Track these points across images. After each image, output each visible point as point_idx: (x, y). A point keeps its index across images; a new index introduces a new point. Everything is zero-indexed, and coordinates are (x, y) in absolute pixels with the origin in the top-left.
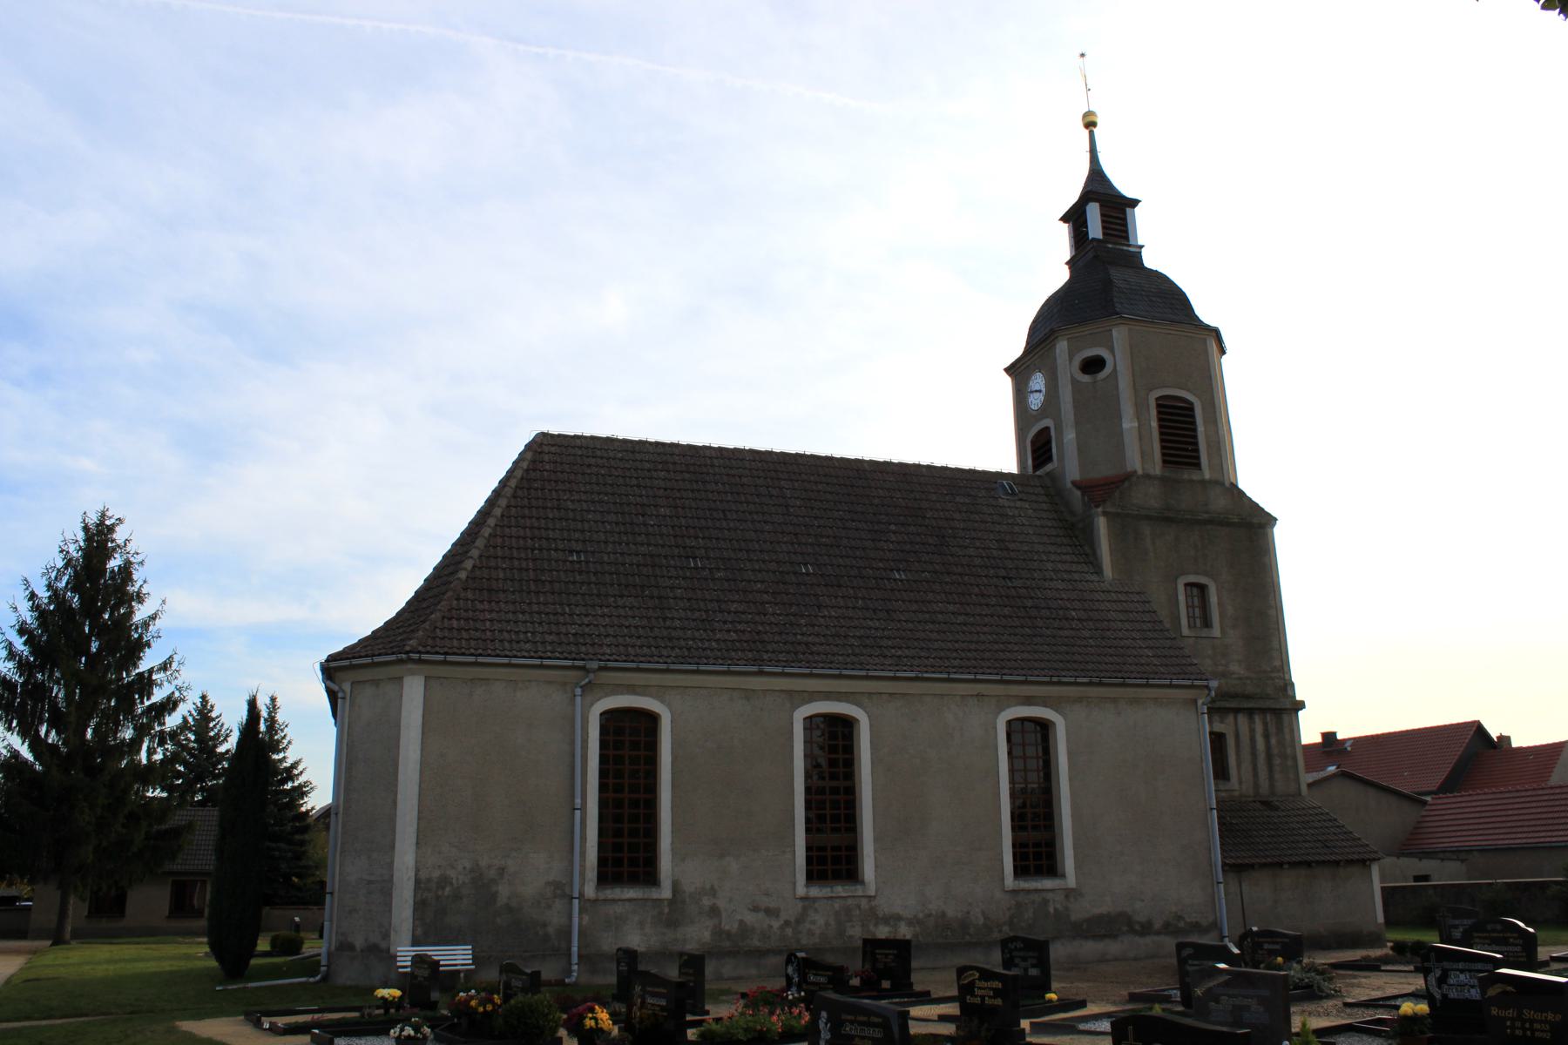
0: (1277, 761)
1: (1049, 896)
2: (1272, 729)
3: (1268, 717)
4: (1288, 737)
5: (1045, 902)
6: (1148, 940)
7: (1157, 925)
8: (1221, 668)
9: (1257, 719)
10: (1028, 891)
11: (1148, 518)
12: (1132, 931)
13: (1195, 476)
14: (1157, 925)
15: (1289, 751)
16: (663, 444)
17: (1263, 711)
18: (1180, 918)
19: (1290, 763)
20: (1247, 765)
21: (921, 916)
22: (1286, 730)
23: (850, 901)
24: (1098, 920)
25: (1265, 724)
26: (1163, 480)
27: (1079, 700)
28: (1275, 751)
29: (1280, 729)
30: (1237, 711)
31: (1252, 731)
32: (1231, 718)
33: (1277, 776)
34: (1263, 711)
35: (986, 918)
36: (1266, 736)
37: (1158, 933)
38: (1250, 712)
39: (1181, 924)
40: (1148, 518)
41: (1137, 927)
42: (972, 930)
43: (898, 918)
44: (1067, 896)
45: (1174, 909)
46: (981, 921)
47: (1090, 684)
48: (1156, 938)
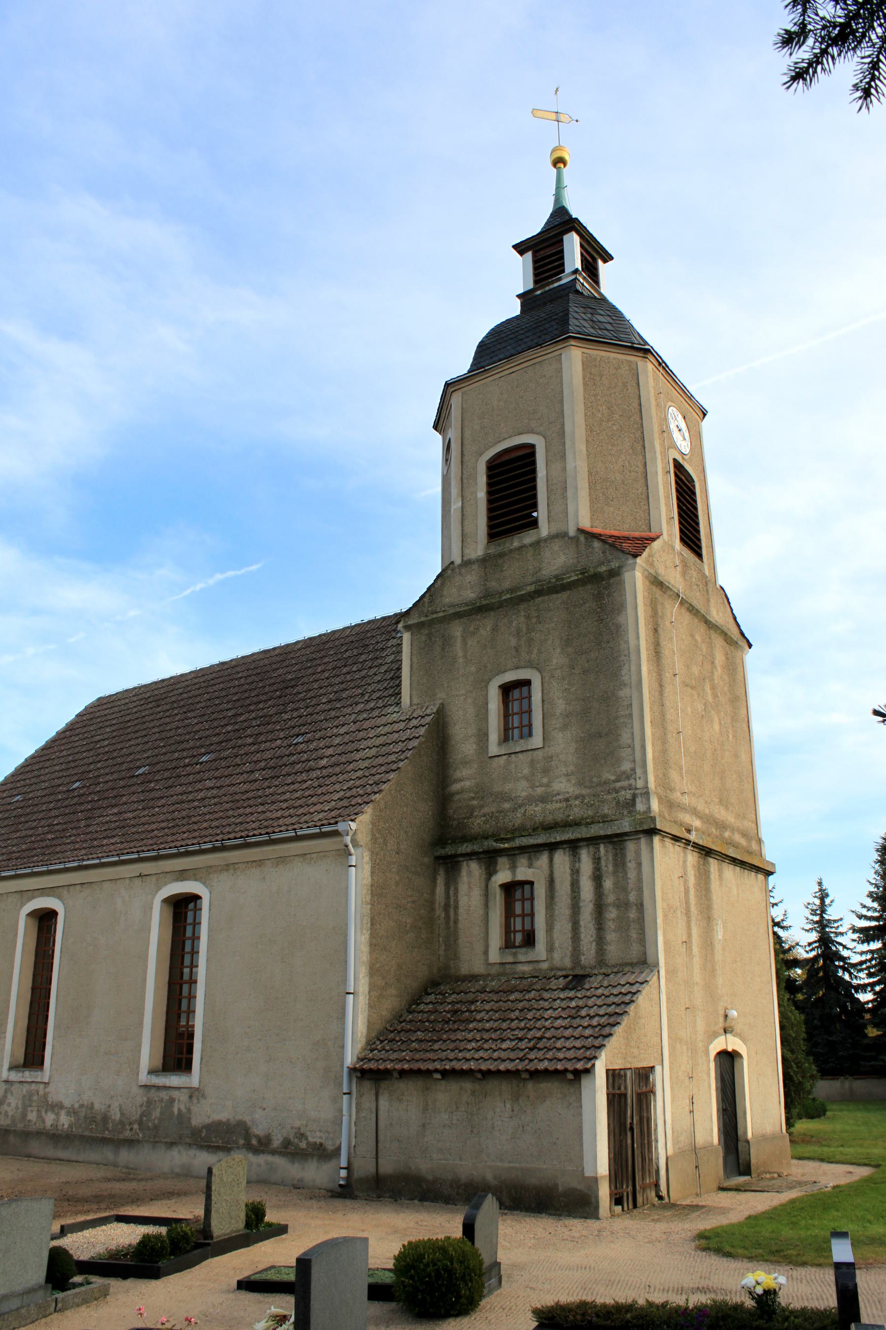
0: (612, 914)
1: (175, 1094)
2: (608, 866)
3: (602, 848)
4: (632, 875)
5: (172, 1100)
6: (262, 1159)
7: (276, 1143)
8: (540, 790)
9: (585, 856)
10: (158, 1088)
11: (458, 615)
12: (249, 1147)
13: (528, 537)
14: (276, 1143)
15: (632, 897)
16: (145, 686)
17: (593, 841)
18: (302, 1136)
19: (633, 914)
20: (563, 927)
21: (77, 1106)
22: (631, 865)
23: (33, 1086)
24: (216, 1128)
25: (597, 860)
26: (484, 561)
27: (227, 867)
28: (610, 898)
29: (620, 863)
30: (552, 847)
31: (575, 873)
32: (544, 859)
33: (611, 936)
34: (593, 841)
35: (122, 1114)
36: (597, 879)
37: (274, 1152)
38: (573, 846)
39: (303, 1145)
40: (458, 615)
41: (254, 1142)
42: (110, 1126)
43: (61, 1106)
44: (191, 1097)
45: (297, 1124)
46: (118, 1117)
47: (214, 850)
48: (270, 1158)
